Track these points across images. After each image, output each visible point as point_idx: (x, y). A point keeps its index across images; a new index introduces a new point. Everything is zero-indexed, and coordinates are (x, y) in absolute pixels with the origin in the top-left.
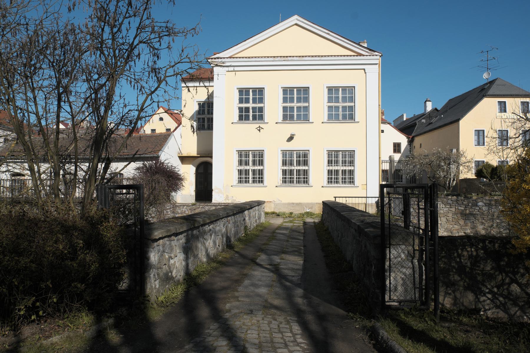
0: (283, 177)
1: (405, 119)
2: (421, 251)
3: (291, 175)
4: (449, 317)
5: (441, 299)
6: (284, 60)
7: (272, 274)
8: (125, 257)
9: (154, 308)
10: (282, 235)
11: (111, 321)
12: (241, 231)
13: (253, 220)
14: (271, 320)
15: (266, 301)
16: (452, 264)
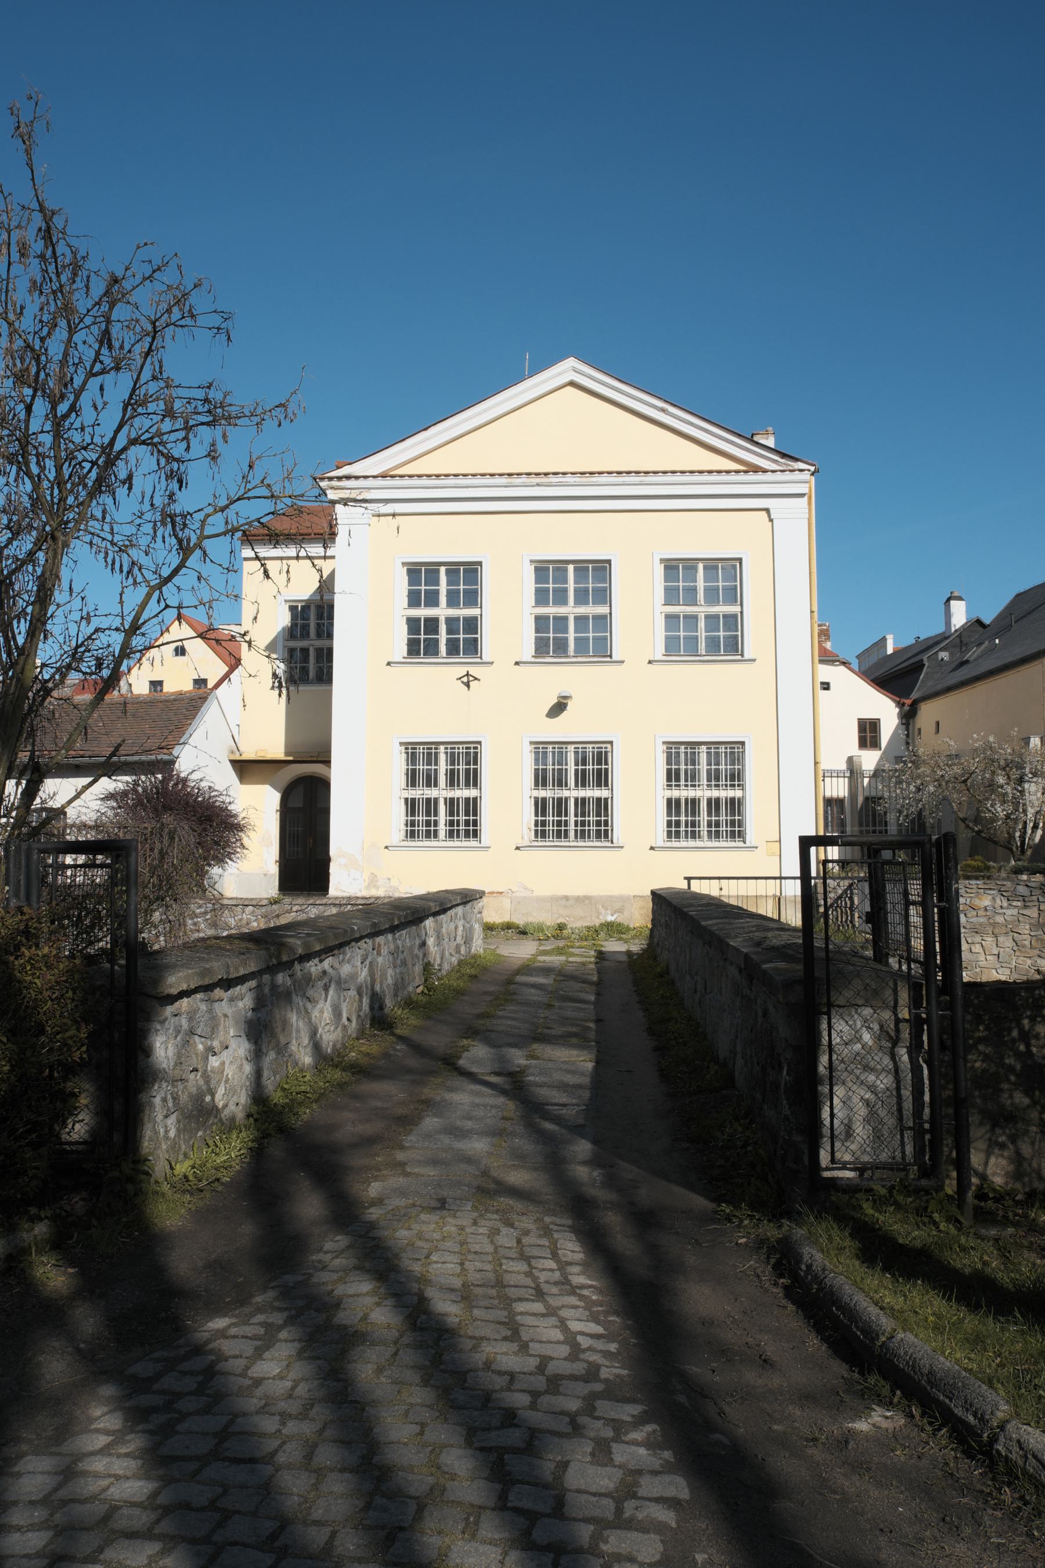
0: (536, 822)
1: (890, 651)
2: (916, 1024)
3: (559, 815)
4: (1001, 1213)
5: (976, 1159)
6: (538, 485)
7: (501, 1100)
8: (83, 1045)
9: (163, 1194)
10: (533, 991)
11: (41, 1229)
12: (414, 980)
13: (449, 947)
14: (499, 1224)
15: (485, 1173)
16: (1007, 1061)
